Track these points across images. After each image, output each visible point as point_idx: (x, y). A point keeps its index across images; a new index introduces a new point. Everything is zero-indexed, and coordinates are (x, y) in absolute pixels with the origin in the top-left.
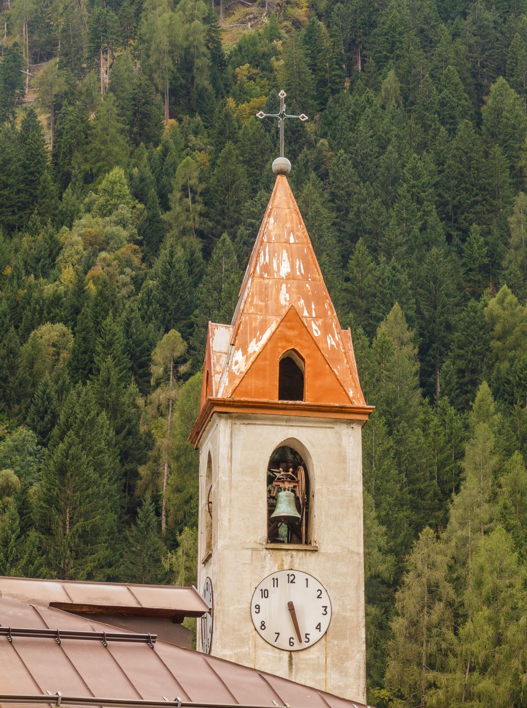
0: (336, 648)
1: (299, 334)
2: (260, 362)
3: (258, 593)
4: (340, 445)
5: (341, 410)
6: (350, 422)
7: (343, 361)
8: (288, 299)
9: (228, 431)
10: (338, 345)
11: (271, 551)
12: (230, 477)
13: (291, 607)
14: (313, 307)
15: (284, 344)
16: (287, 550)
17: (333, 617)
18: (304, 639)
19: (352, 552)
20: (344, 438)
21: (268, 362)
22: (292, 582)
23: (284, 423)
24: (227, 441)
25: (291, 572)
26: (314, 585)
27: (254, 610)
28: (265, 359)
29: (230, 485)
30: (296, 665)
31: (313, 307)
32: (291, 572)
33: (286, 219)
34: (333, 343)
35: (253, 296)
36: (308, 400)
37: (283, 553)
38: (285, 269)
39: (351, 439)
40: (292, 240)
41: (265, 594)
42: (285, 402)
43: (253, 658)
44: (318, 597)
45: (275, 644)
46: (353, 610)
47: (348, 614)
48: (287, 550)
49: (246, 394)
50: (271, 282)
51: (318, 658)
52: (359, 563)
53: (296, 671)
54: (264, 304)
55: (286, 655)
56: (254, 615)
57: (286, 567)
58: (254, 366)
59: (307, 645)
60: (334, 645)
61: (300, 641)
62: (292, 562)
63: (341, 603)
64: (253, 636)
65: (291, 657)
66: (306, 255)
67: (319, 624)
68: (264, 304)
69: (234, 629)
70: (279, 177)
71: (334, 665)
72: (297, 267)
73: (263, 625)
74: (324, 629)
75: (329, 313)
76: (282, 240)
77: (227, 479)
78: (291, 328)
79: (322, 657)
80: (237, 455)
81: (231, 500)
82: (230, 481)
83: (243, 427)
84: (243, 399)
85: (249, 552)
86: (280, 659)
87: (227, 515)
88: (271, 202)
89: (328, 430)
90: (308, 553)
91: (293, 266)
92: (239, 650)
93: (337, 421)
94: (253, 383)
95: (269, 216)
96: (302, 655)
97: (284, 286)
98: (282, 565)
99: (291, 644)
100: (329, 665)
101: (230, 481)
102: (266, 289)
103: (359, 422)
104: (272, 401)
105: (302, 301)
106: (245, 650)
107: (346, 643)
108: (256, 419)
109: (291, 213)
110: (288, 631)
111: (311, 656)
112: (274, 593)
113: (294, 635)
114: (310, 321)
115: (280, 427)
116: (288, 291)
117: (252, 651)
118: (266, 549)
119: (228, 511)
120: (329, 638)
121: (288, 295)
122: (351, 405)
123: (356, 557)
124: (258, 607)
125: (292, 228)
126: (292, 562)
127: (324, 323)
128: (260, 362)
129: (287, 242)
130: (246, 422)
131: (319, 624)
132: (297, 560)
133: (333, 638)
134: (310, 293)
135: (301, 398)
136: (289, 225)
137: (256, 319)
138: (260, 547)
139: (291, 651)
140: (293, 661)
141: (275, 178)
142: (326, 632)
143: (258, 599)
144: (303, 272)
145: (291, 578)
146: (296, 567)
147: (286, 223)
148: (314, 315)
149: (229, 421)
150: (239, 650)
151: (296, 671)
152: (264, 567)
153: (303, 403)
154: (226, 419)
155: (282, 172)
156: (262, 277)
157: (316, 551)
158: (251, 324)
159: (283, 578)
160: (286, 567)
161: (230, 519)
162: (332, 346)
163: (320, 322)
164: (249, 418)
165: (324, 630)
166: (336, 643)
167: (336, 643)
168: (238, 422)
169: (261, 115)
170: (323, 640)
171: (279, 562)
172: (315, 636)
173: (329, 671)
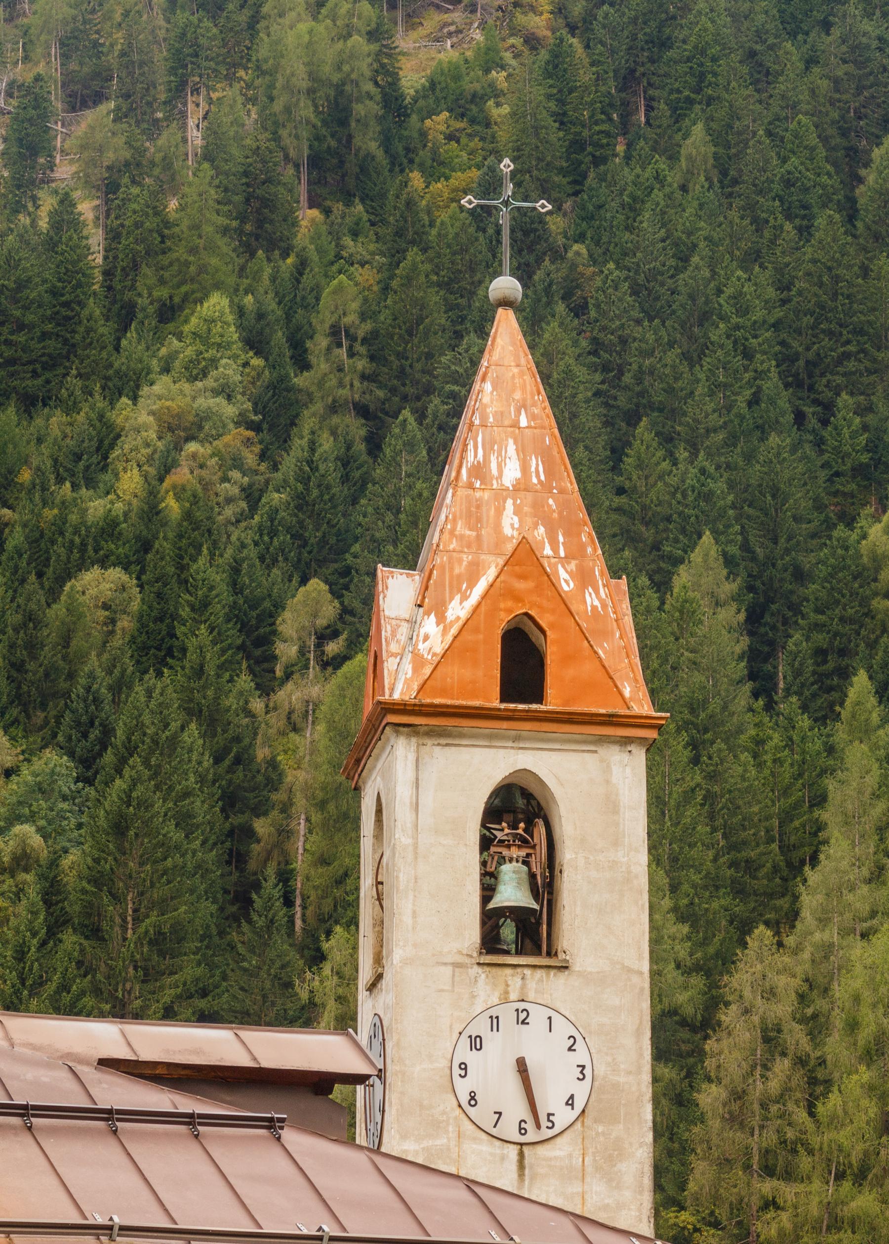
0: (602, 1139)
1: (537, 587)
2: (467, 636)
3: (465, 1042)
4: (608, 782)
5: (610, 720)
6: (625, 742)
7: (613, 634)
9: (412, 757)
10: (604, 606)
11: (487, 969)
12: (415, 838)
15: (510, 604)
19: (629, 970)
20: (616, 770)
21: (481, 637)
22: (523, 1022)
23: (510, 744)
24: (410, 774)
25: (522, 1006)
27: (457, 1071)
28: (476, 630)
30: (531, 1168)
32: (522, 1006)
34: (596, 603)
35: (455, 520)
36: (552, 703)
37: (509, 971)
38: (512, 473)
39: (628, 770)
40: (523, 422)
41: (476, 1043)
42: (512, 706)
44: (570, 1049)
45: (494, 1132)
46: (630, 1073)
47: (622, 1079)
50: (486, 495)
51: (570, 1156)
54: (474, 534)
55: (512, 1152)
57: (513, 996)
58: (457, 643)
59: (550, 1133)
60: (598, 1134)
61: (538, 1126)
62: (523, 987)
64: (456, 1118)
65: (521, 1155)
66: (549, 448)
67: (572, 1097)
68: (474, 534)
70: (500, 310)
72: (533, 469)
73: (473, 1098)
74: (579, 1105)
76: (507, 422)
78: (522, 577)
79: (577, 1153)
80: (427, 800)
82: (416, 846)
83: (437, 749)
84: (437, 701)
86: (503, 1158)
87: (410, 906)
89: (587, 756)
94: (455, 673)
95: (483, 380)
99: (522, 1131)
100: (589, 1169)
101: (416, 846)
102: (478, 507)
105: (542, 530)
106: (442, 1141)
107: (618, 1130)
108: (462, 736)
109: (521, 374)
110: (516, 1109)
111: (558, 1153)
112: (491, 1041)
113: (526, 1114)
116: (517, 511)
117: (453, 1143)
118: (479, 964)
119: (411, 897)
120: (588, 1121)
122: (627, 712)
123: (635, 979)
124: (463, 1066)
125: (524, 400)
126: (523, 987)
128: (467, 636)
129: (516, 425)
130: (443, 741)
131: (572, 1097)
132: (532, 985)
133: (596, 1121)
136: (518, 395)
137: (460, 561)
138: (467, 961)
139: (521, 1144)
140: (527, 1162)
142: (583, 1111)
143: (464, 1053)
144: (543, 478)
145: (523, 1016)
146: (531, 996)
149: (414, 740)
152: (474, 997)
153: (542, 707)
154: (409, 736)
155: (506, 303)
156: (471, 486)
157: (566, 968)
158: (452, 569)
159: (507, 1016)
160: (513, 996)
161: (414, 912)
162: (594, 608)
163: (573, 566)
165: (579, 1106)
168: (429, 742)
169: (470, 202)
170: (578, 1125)
171: (502, 987)
172: (564, 1117)
173: (588, 1179)
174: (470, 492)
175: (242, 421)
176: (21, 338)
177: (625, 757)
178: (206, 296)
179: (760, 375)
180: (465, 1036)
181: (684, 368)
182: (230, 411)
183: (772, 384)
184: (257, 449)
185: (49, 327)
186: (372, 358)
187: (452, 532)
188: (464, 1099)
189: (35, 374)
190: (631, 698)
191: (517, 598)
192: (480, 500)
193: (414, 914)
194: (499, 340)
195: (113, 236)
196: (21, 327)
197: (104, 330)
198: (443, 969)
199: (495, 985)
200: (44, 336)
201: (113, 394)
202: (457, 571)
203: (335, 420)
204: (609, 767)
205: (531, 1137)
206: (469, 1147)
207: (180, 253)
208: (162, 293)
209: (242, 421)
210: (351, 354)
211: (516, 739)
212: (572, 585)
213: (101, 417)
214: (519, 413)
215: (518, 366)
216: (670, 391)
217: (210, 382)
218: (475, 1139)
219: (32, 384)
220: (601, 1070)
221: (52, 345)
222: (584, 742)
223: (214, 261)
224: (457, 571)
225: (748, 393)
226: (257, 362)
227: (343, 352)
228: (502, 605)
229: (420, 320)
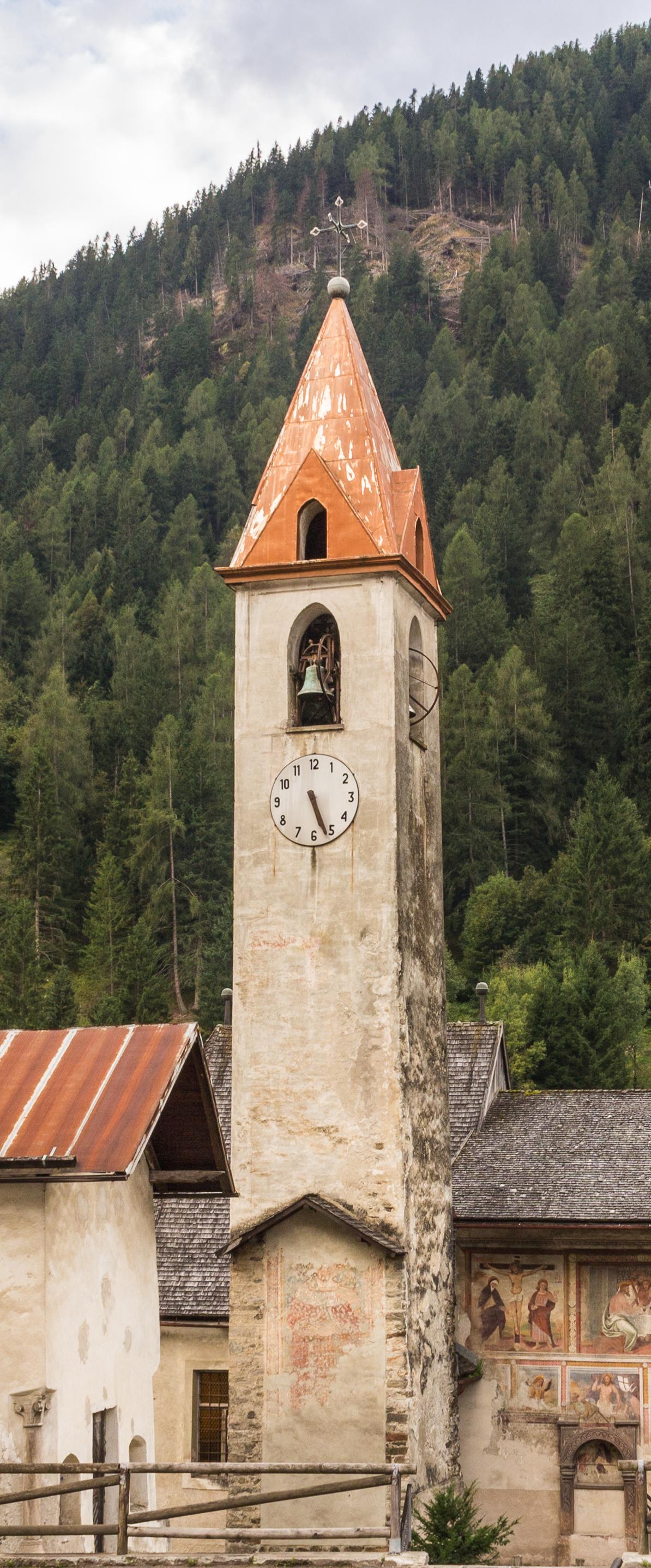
0: (364, 838)
1: (320, 481)
2: (276, 521)
3: (279, 784)
4: (369, 604)
5: (364, 562)
6: (379, 575)
7: (377, 505)
8: (324, 442)
9: (245, 604)
10: (373, 487)
11: (292, 736)
12: (248, 656)
13: (312, 796)
14: (351, 446)
15: (302, 494)
16: (310, 732)
17: (361, 803)
18: (329, 832)
19: (382, 727)
20: (373, 595)
21: (284, 519)
22: (315, 768)
23: (307, 587)
24: (245, 616)
25: (314, 757)
26: (340, 769)
27: (274, 803)
28: (282, 515)
29: (248, 666)
30: (320, 860)
31: (351, 446)
32: (314, 757)
33: (335, 349)
34: (369, 486)
35: (284, 445)
36: (331, 556)
37: (306, 736)
38: (325, 407)
39: (382, 594)
40: (337, 373)
41: (285, 784)
42: (312, 561)
43: (272, 857)
44: (344, 782)
45: (296, 840)
46: (383, 794)
47: (378, 799)
48: (310, 732)
49: (261, 560)
50: (307, 426)
51: (344, 851)
52: (391, 738)
53: (320, 868)
54: (295, 452)
55: (308, 852)
56: (274, 809)
57: (309, 752)
58: (269, 526)
59: (332, 838)
60: (362, 836)
61: (325, 833)
62: (315, 745)
63: (369, 786)
64: (274, 834)
65: (314, 853)
66: (352, 387)
67: (345, 813)
68: (295, 452)
69: (252, 828)
70: (334, 301)
71: (361, 858)
72: (339, 403)
73: (283, 820)
74: (350, 818)
75: (369, 451)
76: (327, 375)
77: (245, 659)
78: (310, 476)
79: (349, 849)
80: (255, 630)
81: (248, 683)
82: (248, 661)
83: (261, 597)
84: (258, 565)
85: (269, 739)
86: (302, 856)
87: (245, 700)
88: (320, 333)
89: (355, 588)
90: (333, 733)
91: (334, 404)
92: (258, 850)
93: (364, 577)
94: (268, 545)
95: (316, 349)
96: (326, 849)
97: (321, 427)
98: (305, 750)
99: (314, 838)
100: (356, 859)
101: (248, 661)
102: (300, 434)
103: (390, 574)
104: (289, 563)
105: (339, 442)
106: (264, 849)
107: (375, 832)
108: (276, 586)
109: (341, 341)
110: (310, 824)
111: (337, 850)
112: (296, 783)
113: (314, 825)
114: (345, 465)
115: (301, 593)
116: (326, 433)
117: (271, 850)
118: (288, 733)
119: (245, 695)
120: (356, 827)
121: (324, 438)
122: (378, 555)
123: (386, 732)
124: (277, 800)
125: (340, 358)
126: (315, 745)
127: (361, 465)
128: (276, 521)
129: (332, 376)
130: (264, 591)
131: (345, 813)
132: (320, 743)
133: (361, 827)
134: (350, 431)
135: (325, 557)
136: (336, 356)
137: (284, 472)
138: (281, 732)
139: (314, 847)
140: (317, 858)
141: (330, 302)
142: (353, 821)
143: (279, 792)
144: (345, 408)
145: (314, 764)
146: (320, 750)
147: (334, 353)
148: (350, 456)
149: (246, 593)
150: (258, 850)
151: (320, 868)
152: (284, 755)
153: (327, 559)
154: (243, 591)
155: (338, 294)
156: (298, 421)
157: (342, 729)
158: (278, 478)
159: (305, 764)
160: (309, 752)
161: (247, 704)
162: (366, 489)
163: (356, 464)
164: (268, 587)
165: (350, 818)
166: (364, 832)
167: (364, 832)
168: (256, 593)
169: (316, 231)
170: (350, 831)
171: (301, 748)
172: (340, 826)
173: (355, 865)
174: (297, 425)
177: (380, 585)
180: (278, 781)
187: (281, 454)
188: (278, 820)
190: (382, 547)
191: (308, 490)
192: (302, 429)
193: (248, 706)
194: (330, 322)
198: (265, 738)
199: (298, 746)
202: (281, 478)
204: (369, 594)
205: (321, 839)
206: (281, 851)
211: (311, 583)
212: (354, 476)
214: (335, 367)
215: (340, 336)
218: (284, 846)
220: (364, 794)
222: (354, 579)
224: (281, 478)
228: (298, 497)
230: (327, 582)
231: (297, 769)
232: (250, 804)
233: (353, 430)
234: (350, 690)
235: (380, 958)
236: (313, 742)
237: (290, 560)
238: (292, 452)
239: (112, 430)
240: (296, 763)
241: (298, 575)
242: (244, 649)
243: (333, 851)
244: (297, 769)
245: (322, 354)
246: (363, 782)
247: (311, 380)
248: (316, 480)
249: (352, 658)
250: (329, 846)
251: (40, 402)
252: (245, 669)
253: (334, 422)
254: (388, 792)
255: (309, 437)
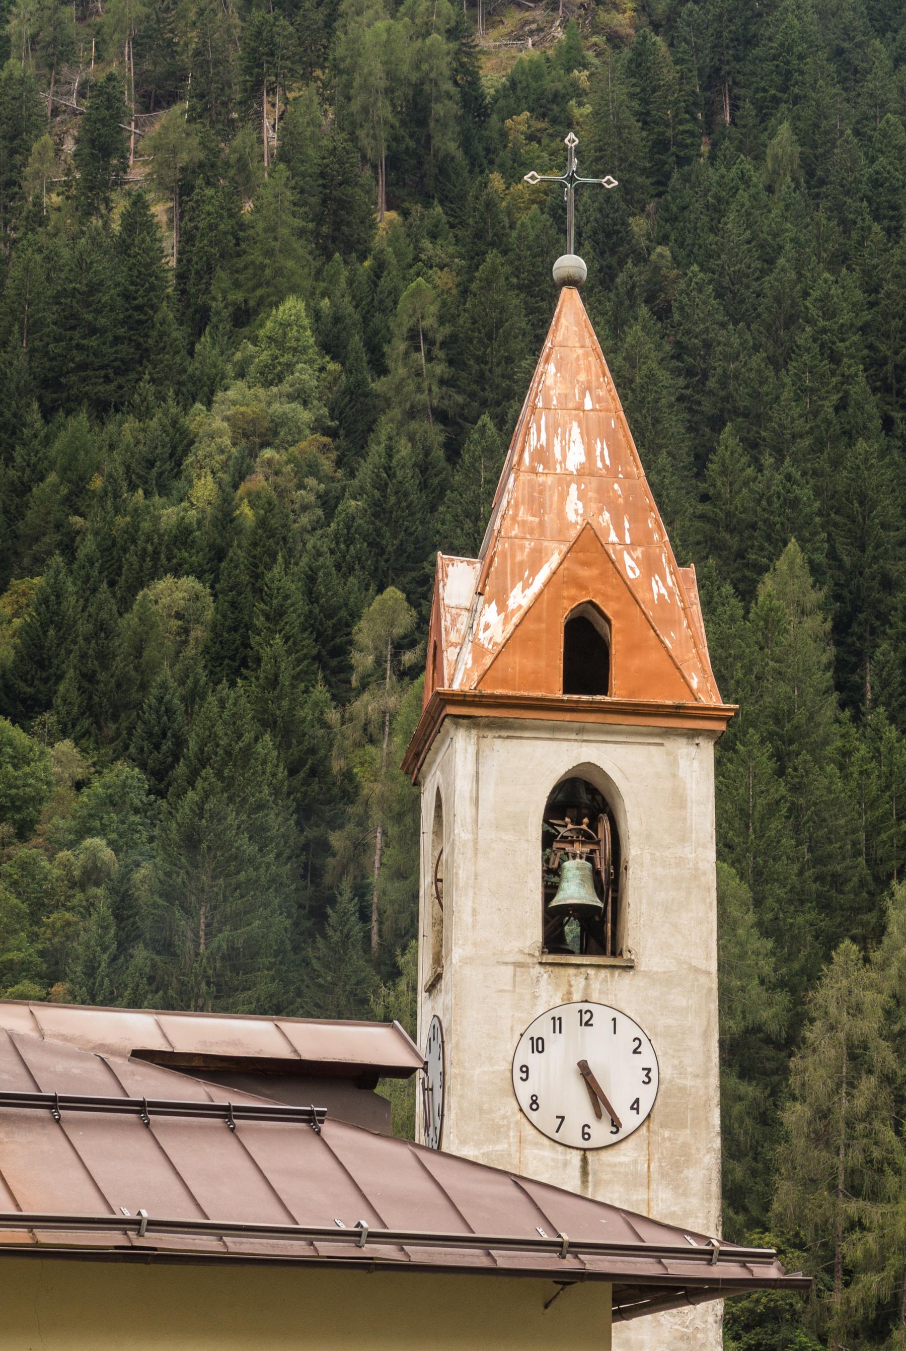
1: (602, 574)
2: (529, 626)
3: (526, 1044)
4: (674, 776)
5: (677, 712)
6: (692, 734)
8: (581, 511)
9: (472, 749)
10: (671, 594)
11: (550, 969)
12: (475, 834)
15: (573, 591)
17: (662, 1087)
19: (697, 970)
20: (683, 763)
21: (544, 626)
23: (574, 737)
24: (471, 767)
25: (585, 1007)
27: (518, 1074)
28: (539, 619)
30: (595, 1174)
32: (585, 1007)
34: (663, 591)
35: (517, 506)
36: (617, 694)
37: (571, 971)
38: (576, 457)
39: (696, 764)
40: (588, 404)
41: (538, 1045)
42: (575, 697)
44: (635, 1052)
45: (557, 1137)
46: (697, 1076)
47: (689, 1083)
49: (504, 683)
50: (549, 480)
51: (635, 1162)
54: (537, 520)
57: (576, 997)
58: (518, 633)
60: (664, 1139)
62: (587, 987)
63: (676, 1062)
64: (517, 1123)
65: (584, 1160)
68: (537, 520)
69: (481, 1110)
70: (565, 290)
71: (664, 1175)
72: (598, 453)
73: (534, 1102)
74: (645, 1109)
76: (571, 405)
78: (586, 564)
79: (643, 1159)
80: (488, 793)
81: (476, 876)
82: (476, 841)
83: (498, 742)
84: (498, 692)
86: (565, 1164)
87: (470, 903)
90: (617, 972)
91: (589, 452)
95: (547, 361)
97: (573, 488)
98: (569, 993)
99: (586, 1136)
100: (655, 1175)
101: (476, 841)
102: (541, 492)
104: (550, 696)
105: (607, 515)
107: (685, 1135)
108: (524, 728)
109: (586, 355)
111: (622, 1159)
112: (555, 1044)
115: (565, 744)
116: (581, 497)
117: (514, 1149)
118: (541, 963)
119: (471, 895)
120: (654, 1125)
121: (580, 505)
123: (703, 979)
124: (525, 1069)
126: (587, 987)
128: (529, 626)
129: (580, 407)
130: (504, 733)
132: (596, 985)
133: (662, 1126)
134: (621, 501)
135: (604, 691)
137: (522, 548)
138: (529, 960)
139: (585, 1150)
142: (649, 1116)
143: (526, 1056)
144: (608, 462)
145: (586, 1017)
146: (595, 997)
148: (628, 541)
149: (474, 732)
152: (536, 997)
154: (469, 728)
155: (570, 282)
156: (533, 471)
157: (631, 967)
158: (513, 556)
159: (570, 1017)
160: (576, 997)
162: (661, 596)
163: (638, 553)
166: (667, 1134)
167: (667, 1134)
168: (490, 734)
170: (644, 1130)
171: (564, 989)
173: (654, 1186)
174: (533, 476)
175: (318, 427)
176: (93, 342)
178: (282, 300)
179: (847, 379)
181: (770, 372)
182: (306, 416)
183: (860, 388)
184: (334, 455)
185: (121, 331)
186: (451, 362)
187: (514, 518)
188: (526, 1103)
189: (107, 380)
190: (699, 690)
191: (581, 586)
193: (474, 912)
194: (563, 321)
195: (187, 238)
196: (93, 331)
197: (178, 334)
199: (558, 985)
200: (117, 340)
201: (187, 400)
202: (519, 558)
203: (413, 425)
207: (256, 256)
208: (237, 296)
209: (318, 427)
210: (430, 358)
213: (174, 423)
215: (582, 347)
216: (755, 395)
217: (285, 388)
219: (104, 390)
220: (667, 1073)
221: (125, 350)
223: (290, 264)
224: (519, 558)
225: (835, 398)
226: (333, 366)
227: (421, 357)
229: (500, 324)
230: (608, 733)
231: (557, 1023)
232: (478, 1071)
233: (626, 499)
234: (644, 907)
235: (695, 1338)
236: (582, 982)
237: (552, 692)
238: (530, 518)
239: (265, 445)
240: (556, 1013)
241: (568, 716)
242: (469, 820)
243: (617, 1160)
244: (557, 1023)
245: (558, 370)
246: (665, 1054)
247: (547, 408)
248: (594, 572)
249: (647, 858)
250: (611, 1152)
251: (111, 375)
252: (470, 853)
253: (594, 482)
254: (706, 1075)
255: (555, 498)
